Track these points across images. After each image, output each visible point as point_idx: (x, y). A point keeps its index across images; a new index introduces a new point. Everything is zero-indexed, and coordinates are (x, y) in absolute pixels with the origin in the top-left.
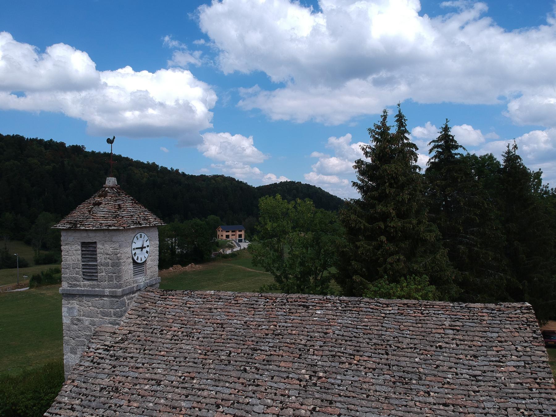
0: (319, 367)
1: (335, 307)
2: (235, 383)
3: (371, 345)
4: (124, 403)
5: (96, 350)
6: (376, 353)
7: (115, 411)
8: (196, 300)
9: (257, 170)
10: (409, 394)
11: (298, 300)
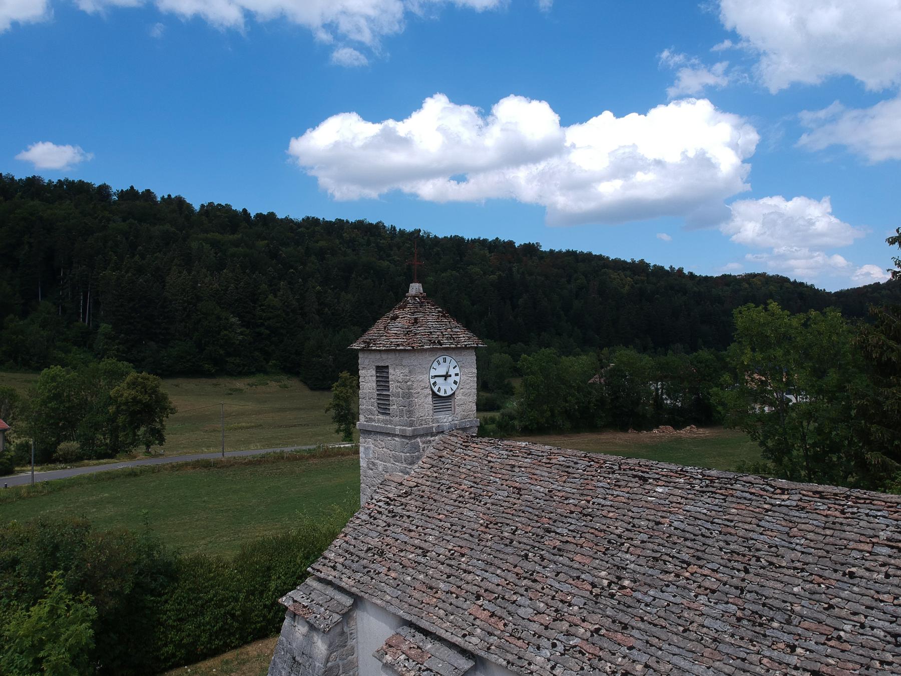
0: (628, 572)
1: (689, 484)
2: (509, 571)
3: (725, 552)
4: (384, 570)
5: (377, 502)
6: (728, 567)
7: (372, 578)
8: (501, 452)
9: (839, 260)
10: (758, 642)
11: (636, 468)
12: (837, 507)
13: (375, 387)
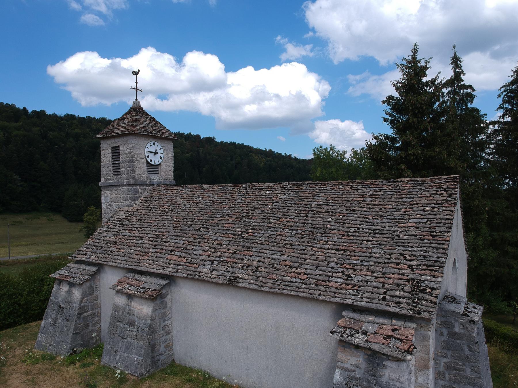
1: (282, 188)
3: (297, 211)
5: (113, 221)
12: (348, 186)
13: (111, 160)
